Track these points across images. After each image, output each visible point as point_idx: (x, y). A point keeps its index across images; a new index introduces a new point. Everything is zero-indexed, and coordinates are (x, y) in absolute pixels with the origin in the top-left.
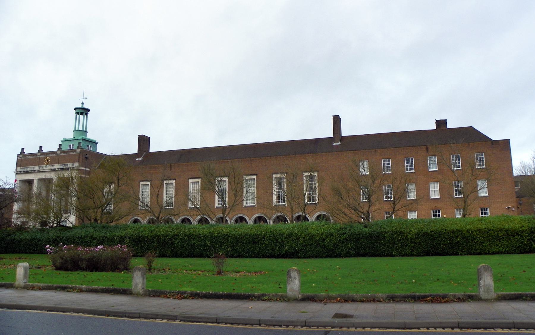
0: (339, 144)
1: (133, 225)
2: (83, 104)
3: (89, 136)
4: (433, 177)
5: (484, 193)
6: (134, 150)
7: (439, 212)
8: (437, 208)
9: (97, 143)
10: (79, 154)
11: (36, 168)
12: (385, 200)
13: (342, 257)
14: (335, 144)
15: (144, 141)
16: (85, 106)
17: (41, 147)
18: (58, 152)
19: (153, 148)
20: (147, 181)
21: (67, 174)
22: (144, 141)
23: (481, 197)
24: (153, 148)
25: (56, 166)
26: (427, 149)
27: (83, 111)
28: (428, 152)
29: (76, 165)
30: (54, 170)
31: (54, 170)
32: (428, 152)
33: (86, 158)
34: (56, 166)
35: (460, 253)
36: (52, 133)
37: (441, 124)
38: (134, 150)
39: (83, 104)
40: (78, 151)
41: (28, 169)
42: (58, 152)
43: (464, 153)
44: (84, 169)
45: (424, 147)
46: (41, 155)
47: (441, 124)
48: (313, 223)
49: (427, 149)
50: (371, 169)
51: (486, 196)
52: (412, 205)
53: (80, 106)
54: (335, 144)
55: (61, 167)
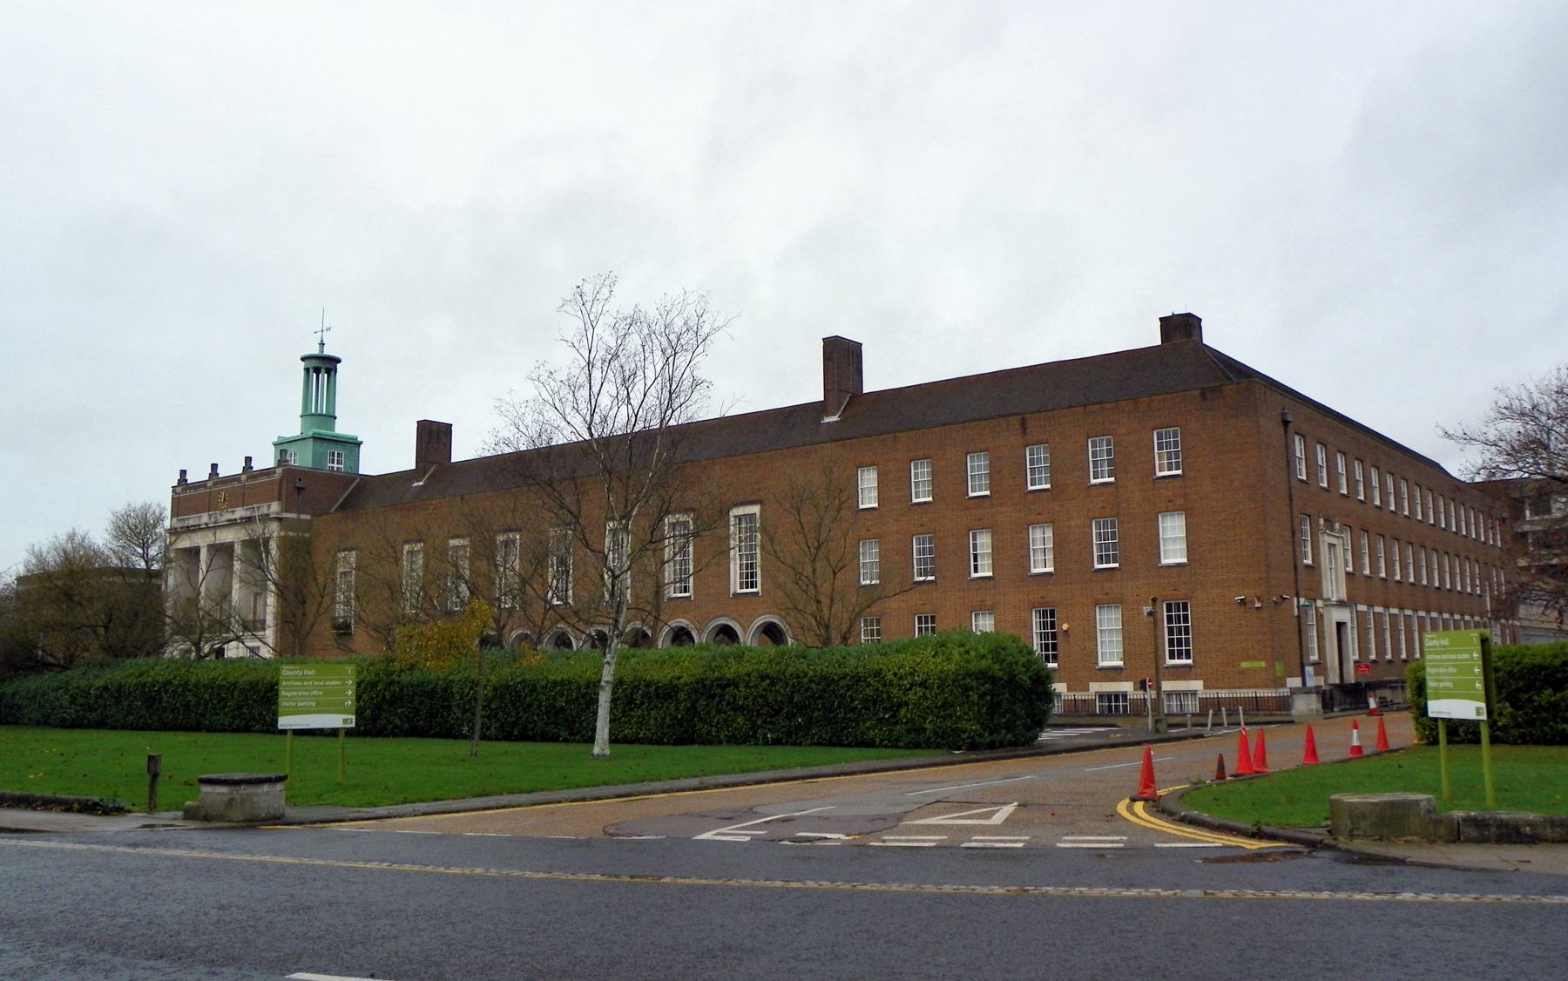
0: (835, 418)
1: (674, 650)
2: (322, 344)
3: (342, 428)
4: (1037, 509)
5: (1174, 553)
6: (811, 390)
7: (1185, 609)
8: (1046, 604)
9: (359, 444)
10: (281, 480)
11: (205, 518)
12: (1098, 566)
13: (387, 736)
14: (827, 420)
15: (842, 357)
16: (327, 352)
17: (214, 467)
18: (244, 478)
19: (876, 379)
20: (686, 511)
21: (258, 528)
22: (842, 357)
23: (1169, 567)
24: (876, 379)
25: (240, 513)
26: (1023, 426)
27: (323, 366)
28: (1025, 433)
29: (275, 507)
30: (233, 523)
31: (233, 523)
32: (1025, 433)
33: (299, 489)
34: (240, 513)
35: (564, 734)
36: (252, 429)
37: (1181, 328)
38: (811, 390)
39: (322, 344)
40: (279, 471)
41: (191, 522)
42: (244, 478)
43: (1122, 430)
44: (294, 516)
45: (1015, 421)
46: (215, 484)
47: (1181, 328)
48: (703, 648)
49: (1023, 426)
50: (1054, 473)
51: (1179, 565)
52: (982, 596)
53: (316, 351)
54: (827, 420)
55: (248, 514)
